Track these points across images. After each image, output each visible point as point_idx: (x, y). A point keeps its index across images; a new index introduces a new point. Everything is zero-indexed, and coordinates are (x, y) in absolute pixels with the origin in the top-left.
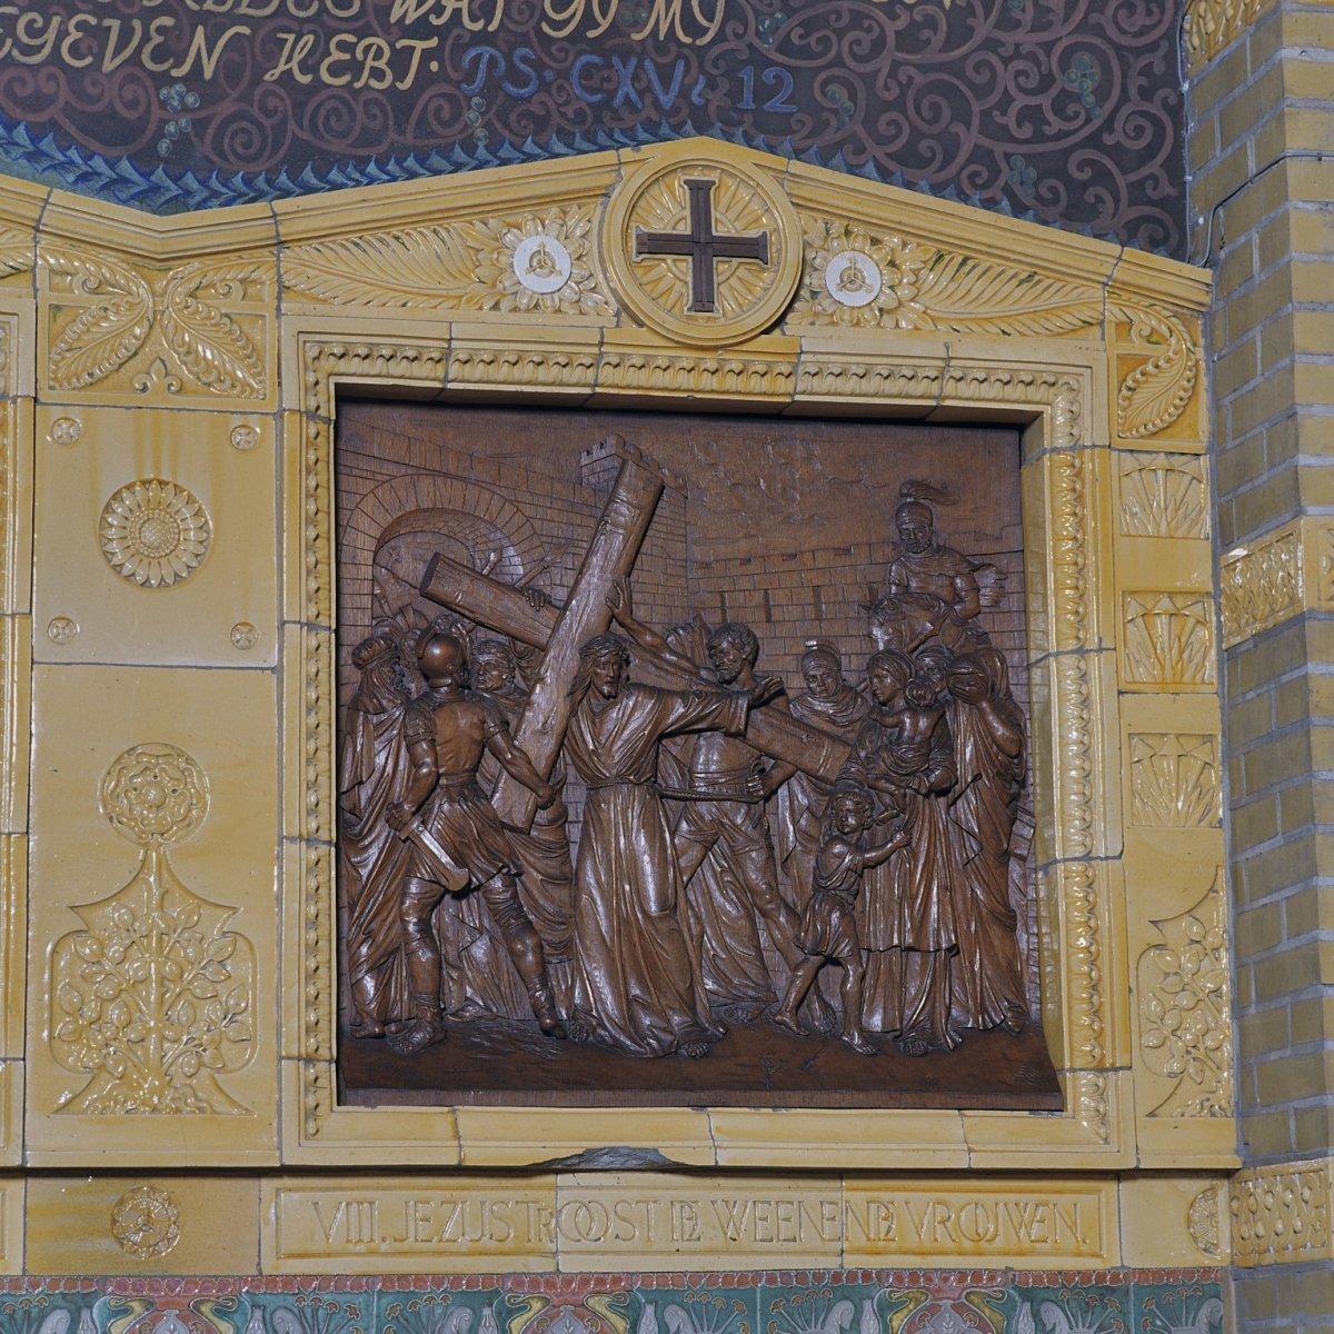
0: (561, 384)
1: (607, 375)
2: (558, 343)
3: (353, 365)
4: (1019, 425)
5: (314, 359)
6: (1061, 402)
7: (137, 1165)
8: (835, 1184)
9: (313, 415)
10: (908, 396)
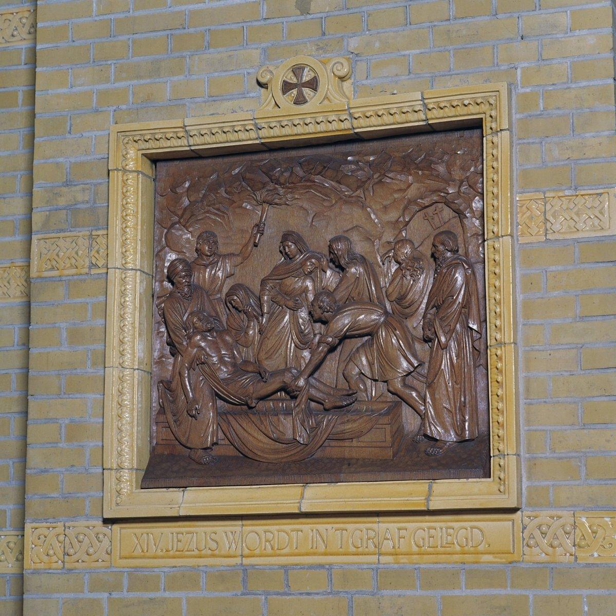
1: (264, 133)
2: (244, 120)
3: (151, 144)
4: (476, 125)
5: (489, 102)
7: (447, 508)
8: (376, 519)
10: (232, 142)
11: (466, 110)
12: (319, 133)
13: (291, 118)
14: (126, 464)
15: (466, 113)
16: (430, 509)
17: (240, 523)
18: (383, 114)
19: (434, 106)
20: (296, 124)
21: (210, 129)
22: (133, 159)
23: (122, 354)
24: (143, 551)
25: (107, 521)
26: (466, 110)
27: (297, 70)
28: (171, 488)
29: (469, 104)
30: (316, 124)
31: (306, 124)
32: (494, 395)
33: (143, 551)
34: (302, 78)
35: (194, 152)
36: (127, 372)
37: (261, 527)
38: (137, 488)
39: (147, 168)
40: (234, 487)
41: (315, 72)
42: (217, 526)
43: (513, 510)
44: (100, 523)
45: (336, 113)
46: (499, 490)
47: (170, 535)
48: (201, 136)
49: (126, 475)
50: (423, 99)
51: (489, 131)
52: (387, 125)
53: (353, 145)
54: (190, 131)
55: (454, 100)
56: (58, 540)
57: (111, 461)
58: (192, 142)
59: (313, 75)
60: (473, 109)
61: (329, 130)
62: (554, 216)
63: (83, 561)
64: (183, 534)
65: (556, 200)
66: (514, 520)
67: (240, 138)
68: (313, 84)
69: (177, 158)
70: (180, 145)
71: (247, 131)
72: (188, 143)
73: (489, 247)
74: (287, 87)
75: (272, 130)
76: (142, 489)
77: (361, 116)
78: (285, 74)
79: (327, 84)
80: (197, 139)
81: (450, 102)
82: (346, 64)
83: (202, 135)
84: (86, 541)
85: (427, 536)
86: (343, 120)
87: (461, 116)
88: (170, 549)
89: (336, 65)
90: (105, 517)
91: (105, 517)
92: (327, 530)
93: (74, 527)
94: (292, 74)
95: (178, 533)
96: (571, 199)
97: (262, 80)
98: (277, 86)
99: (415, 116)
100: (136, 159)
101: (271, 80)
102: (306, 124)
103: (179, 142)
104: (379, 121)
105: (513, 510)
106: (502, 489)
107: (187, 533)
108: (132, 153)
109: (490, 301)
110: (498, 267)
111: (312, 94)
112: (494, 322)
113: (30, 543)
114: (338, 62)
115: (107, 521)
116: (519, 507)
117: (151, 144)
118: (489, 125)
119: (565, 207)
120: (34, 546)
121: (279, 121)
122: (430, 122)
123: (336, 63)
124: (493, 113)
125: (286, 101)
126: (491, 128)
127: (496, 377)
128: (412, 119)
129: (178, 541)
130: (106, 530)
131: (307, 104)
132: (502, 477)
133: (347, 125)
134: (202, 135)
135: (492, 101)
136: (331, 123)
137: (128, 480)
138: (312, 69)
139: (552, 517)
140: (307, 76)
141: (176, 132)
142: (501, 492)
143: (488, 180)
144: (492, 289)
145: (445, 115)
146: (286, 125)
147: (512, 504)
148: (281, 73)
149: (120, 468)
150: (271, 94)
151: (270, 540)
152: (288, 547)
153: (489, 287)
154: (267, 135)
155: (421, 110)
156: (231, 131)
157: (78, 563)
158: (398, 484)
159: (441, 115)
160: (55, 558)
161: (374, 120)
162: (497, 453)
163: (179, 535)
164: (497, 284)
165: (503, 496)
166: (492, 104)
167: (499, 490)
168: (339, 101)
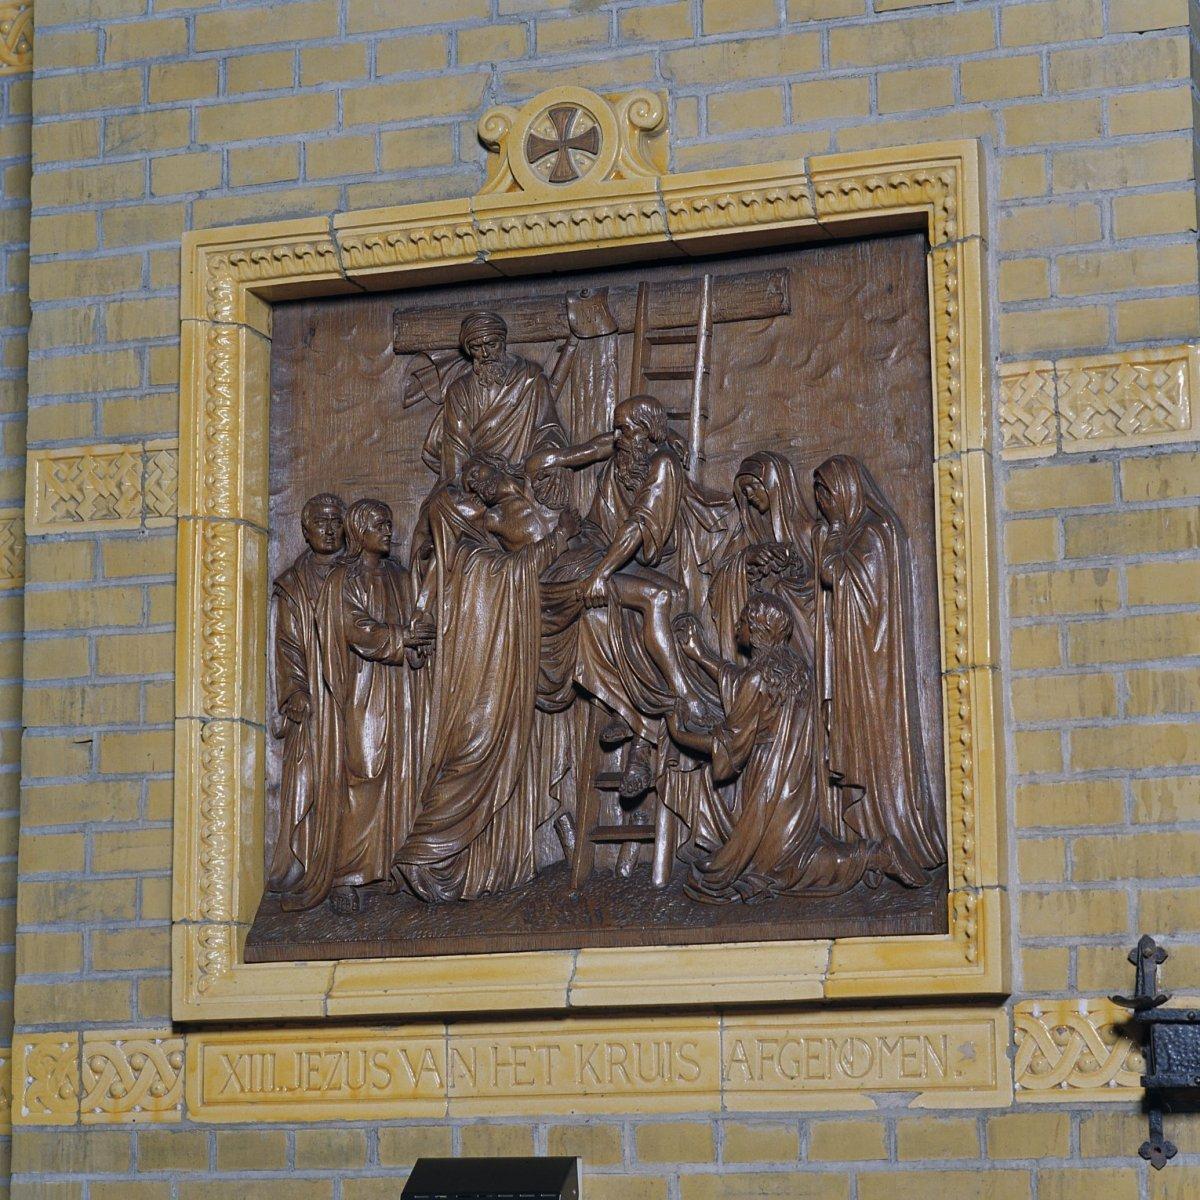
0: (876, 208)
3: (267, 268)
4: (916, 226)
5: (940, 179)
10: (384, 265)
11: (892, 196)
12: (648, 234)
13: (498, 215)
14: (220, 913)
15: (894, 202)
16: (329, 1014)
17: (441, 1029)
18: (729, 204)
19: (830, 189)
20: (555, 223)
21: (691, 200)
22: (230, 296)
23: (209, 687)
24: (242, 1090)
25: (182, 1028)
26: (770, 211)
27: (561, 114)
28: (819, 939)
29: (878, 187)
30: (526, 230)
31: (551, 224)
32: (939, 290)
33: (242, 1090)
34: (567, 131)
35: (355, 283)
36: (219, 727)
37: (423, 1041)
38: (239, 963)
39: (263, 316)
40: (516, 954)
41: (594, 119)
42: (351, 1039)
43: (995, 1000)
44: (167, 1030)
45: (635, 199)
46: (966, 958)
47: (361, 1054)
48: (366, 250)
49: (219, 936)
50: (809, 175)
51: (942, 239)
52: (737, 225)
53: (557, 283)
54: (671, 202)
55: (461, 225)
56: (171, 1064)
57: (186, 904)
58: (347, 261)
59: (590, 124)
60: (909, 193)
61: (622, 235)
62: (1074, 408)
63: (143, 1109)
64: (320, 1054)
65: (1033, 376)
66: (994, 1020)
67: (446, 251)
68: (590, 142)
69: (564, 269)
70: (321, 269)
71: (459, 236)
72: (815, 209)
73: (942, 474)
74: (590, 142)
75: (600, 226)
76: (246, 963)
77: (684, 207)
78: (533, 123)
79: (618, 147)
80: (246, 269)
81: (547, 215)
82: (654, 101)
83: (369, 247)
84: (149, 1068)
85: (804, 1054)
86: (624, 216)
87: (884, 207)
88: (296, 1084)
89: (638, 104)
90: (176, 1018)
91: (174, 1020)
92: (945, 1036)
93: (125, 1041)
94: (548, 124)
95: (309, 1053)
96: (1017, 381)
97: (488, 136)
98: (517, 151)
99: (794, 209)
100: (237, 300)
101: (505, 136)
102: (551, 224)
103: (794, 209)
104: (770, 211)
105: (995, 1000)
106: (972, 954)
107: (327, 1053)
108: (226, 288)
109: (946, 581)
110: (959, 514)
111: (587, 162)
112: (950, 519)
113: (24, 1073)
114: (642, 100)
115: (182, 1028)
116: (1009, 992)
117: (267, 268)
118: (940, 227)
119: (1093, 387)
120: (31, 1079)
121: (312, 243)
122: (824, 220)
123: (634, 103)
124: (950, 202)
125: (535, 177)
126: (946, 233)
127: (959, 732)
128: (787, 214)
129: (311, 1070)
130: (178, 1043)
131: (575, 183)
132: (971, 931)
133: (657, 223)
134: (369, 247)
135: (947, 178)
136: (624, 219)
137: (221, 948)
138: (588, 113)
139: (114, 1042)
140: (579, 126)
141: (455, 226)
142: (970, 961)
143: (942, 441)
144: (950, 556)
145: (853, 207)
146: (536, 224)
147: (996, 988)
148: (528, 121)
149: (206, 920)
150: (506, 163)
151: (621, 1060)
152: (390, 1086)
153: (943, 554)
154: (497, 246)
155: (903, 183)
156: (908, 182)
157: (174, 1112)
158: (755, 948)
159: (845, 207)
160: (166, 1101)
161: (381, 254)
162: (961, 883)
163: (312, 1056)
164: (959, 547)
165: (975, 969)
166: (947, 185)
167: (966, 958)
168: (643, 178)
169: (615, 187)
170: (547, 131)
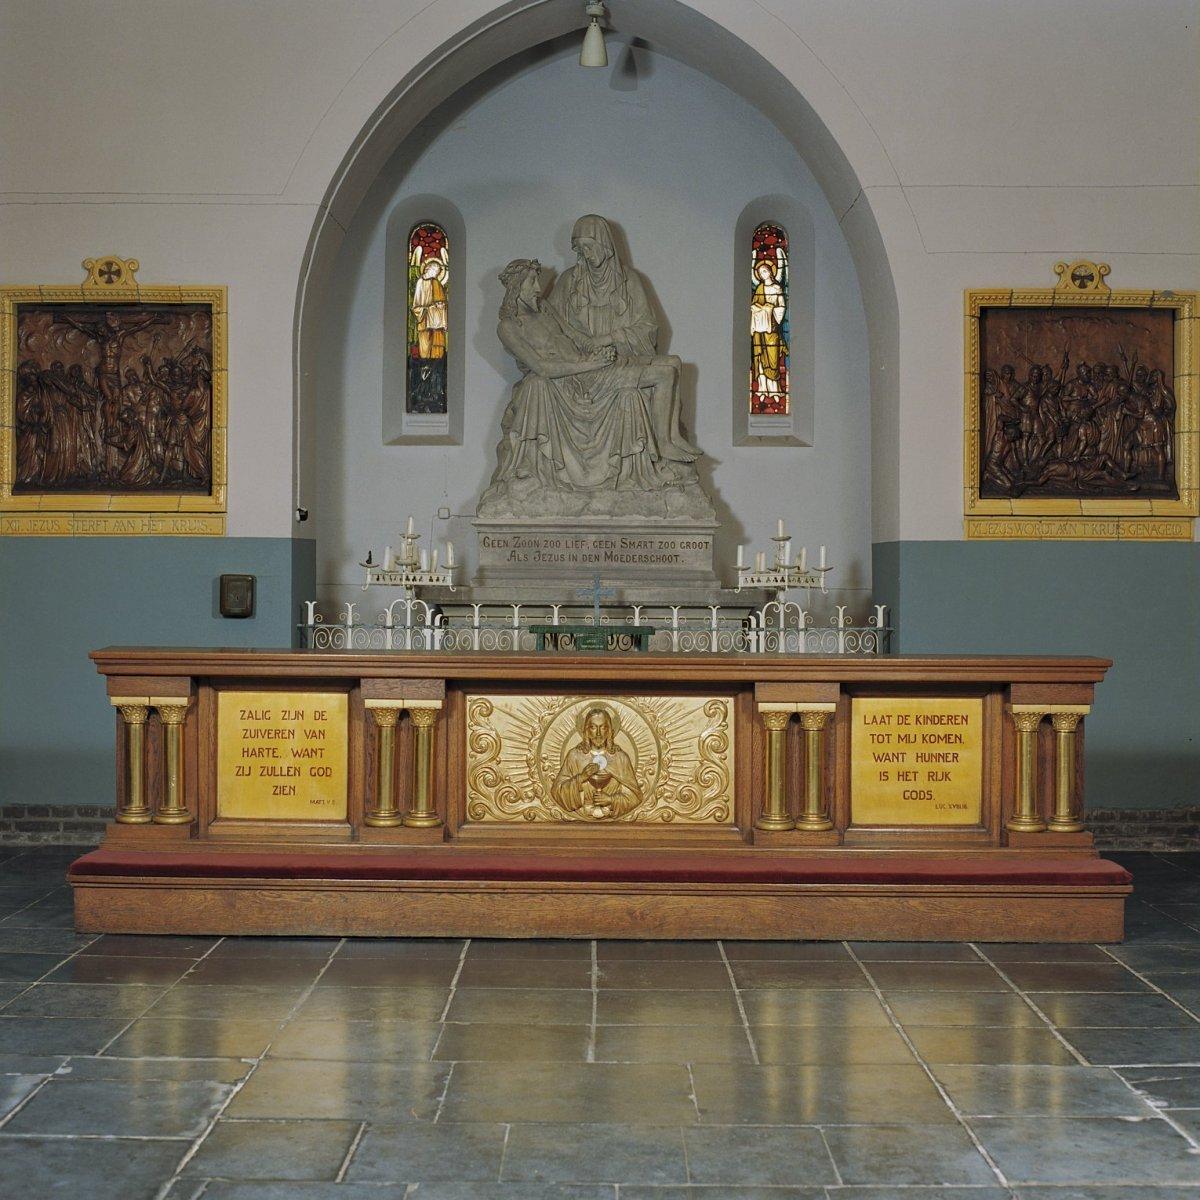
6: (1187, 306)
9: (219, 313)
68: (118, 273)
108: (7, 302)
137: (7, 489)
140: (114, 268)
169: (125, 287)
170: (105, 268)
